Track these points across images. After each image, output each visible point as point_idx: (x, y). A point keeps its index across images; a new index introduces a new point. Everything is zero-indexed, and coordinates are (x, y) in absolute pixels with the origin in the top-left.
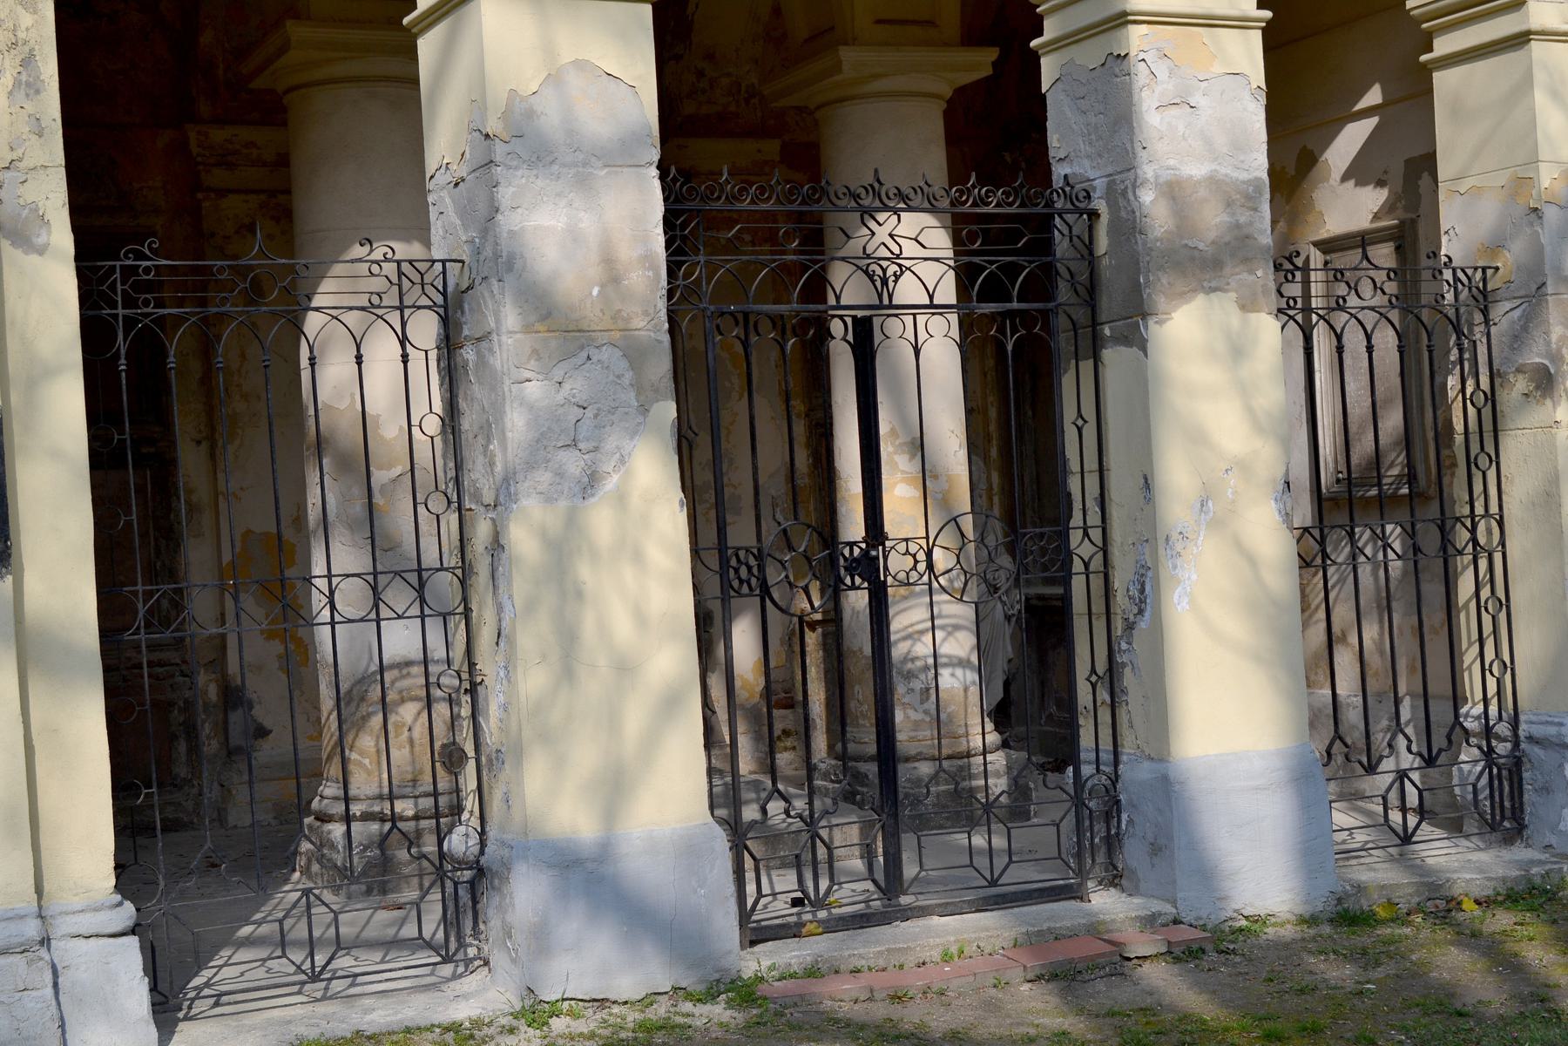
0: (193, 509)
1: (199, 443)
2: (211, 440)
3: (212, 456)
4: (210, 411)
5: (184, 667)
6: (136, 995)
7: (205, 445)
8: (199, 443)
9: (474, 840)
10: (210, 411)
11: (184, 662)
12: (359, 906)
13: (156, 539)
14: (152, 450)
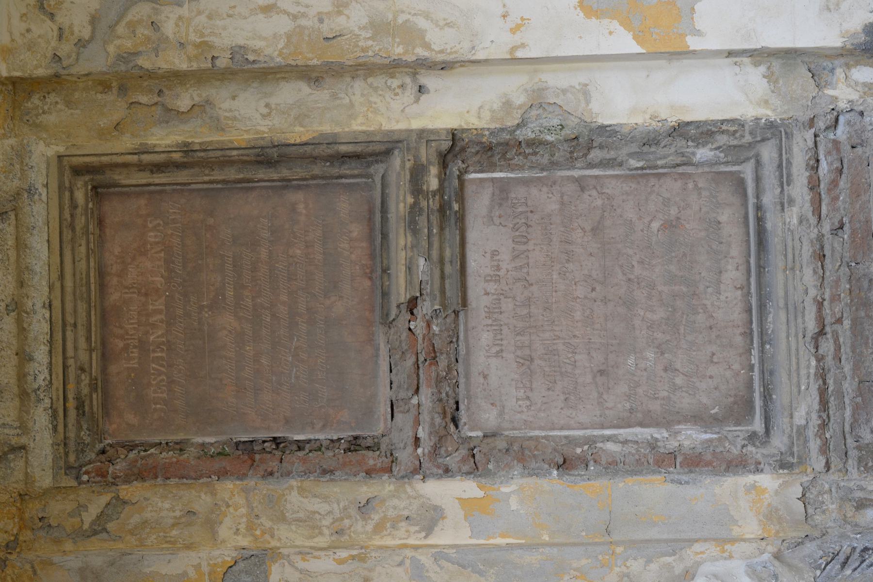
0: (538, 101)
1: (421, 89)
2: (418, 70)
3: (445, 67)
4: (364, 69)
5: (821, 124)
6: (465, 496)
7: (429, 80)
8: (421, 89)
9: (108, 50)
10: (364, 69)
11: (812, 122)
12: (235, 153)
13: (591, 166)
14: (434, 170)
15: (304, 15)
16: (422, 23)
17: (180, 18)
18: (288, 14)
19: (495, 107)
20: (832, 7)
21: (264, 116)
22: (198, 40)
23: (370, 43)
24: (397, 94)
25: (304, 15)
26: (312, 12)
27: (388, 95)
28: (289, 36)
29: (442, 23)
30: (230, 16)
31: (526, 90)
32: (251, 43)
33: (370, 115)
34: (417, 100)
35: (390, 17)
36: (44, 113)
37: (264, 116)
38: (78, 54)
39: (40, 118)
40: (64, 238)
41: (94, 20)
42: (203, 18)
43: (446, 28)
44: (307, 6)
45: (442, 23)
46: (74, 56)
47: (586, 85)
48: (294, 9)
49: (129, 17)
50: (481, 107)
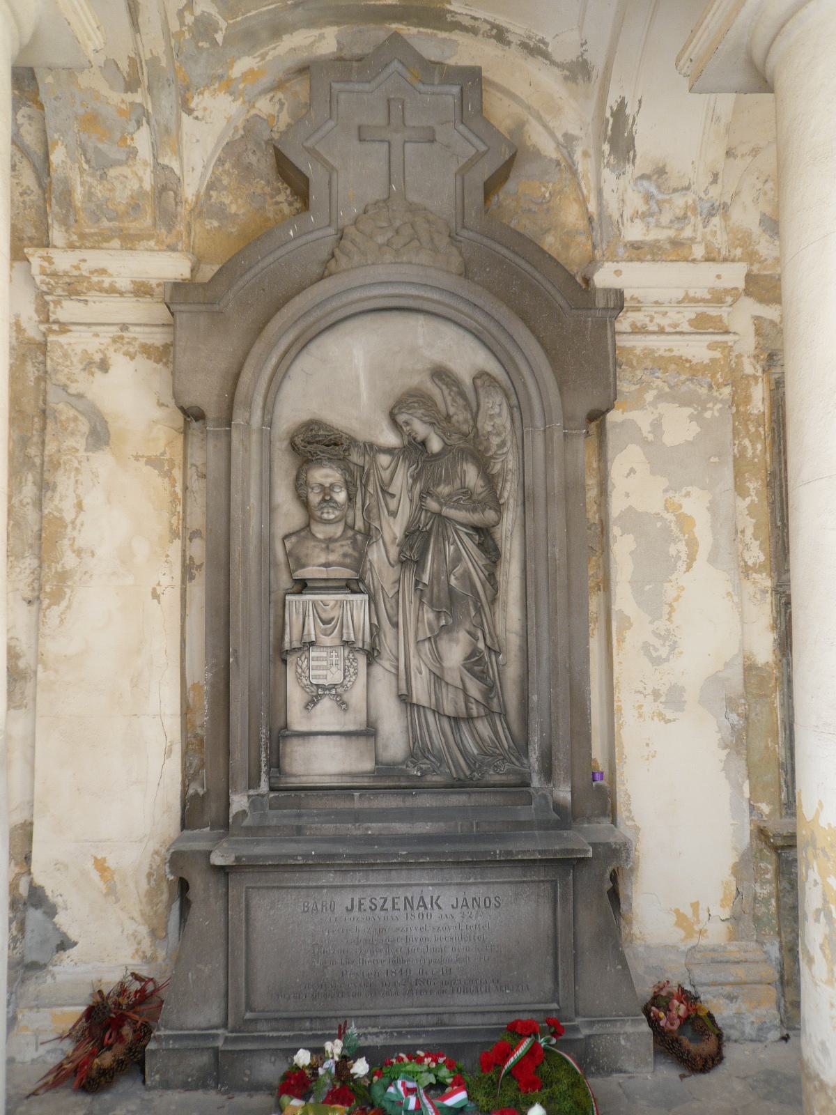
15: (74, 528)
16: (64, 604)
17: (77, 450)
18: (75, 519)
19: (18, 648)
20: (57, 866)
21: (21, 501)
22: (61, 461)
23: (54, 570)
24: (29, 586)
25: (74, 528)
26: (75, 533)
27: (30, 580)
28: (61, 519)
29: (63, 616)
30: (77, 481)
31: (26, 668)
32: (57, 496)
33: (715, 394)
34: (24, 599)
35: (69, 583)
36: (33, 363)
37: (21, 501)
38: (59, 385)
39: (29, 360)
40: (528, 568)
41: (80, 396)
42: (76, 464)
43: (59, 619)
44: (80, 531)
45: (63, 616)
46: (57, 383)
47: (26, 707)
48: (78, 522)
49: (81, 418)
50: (17, 639)
